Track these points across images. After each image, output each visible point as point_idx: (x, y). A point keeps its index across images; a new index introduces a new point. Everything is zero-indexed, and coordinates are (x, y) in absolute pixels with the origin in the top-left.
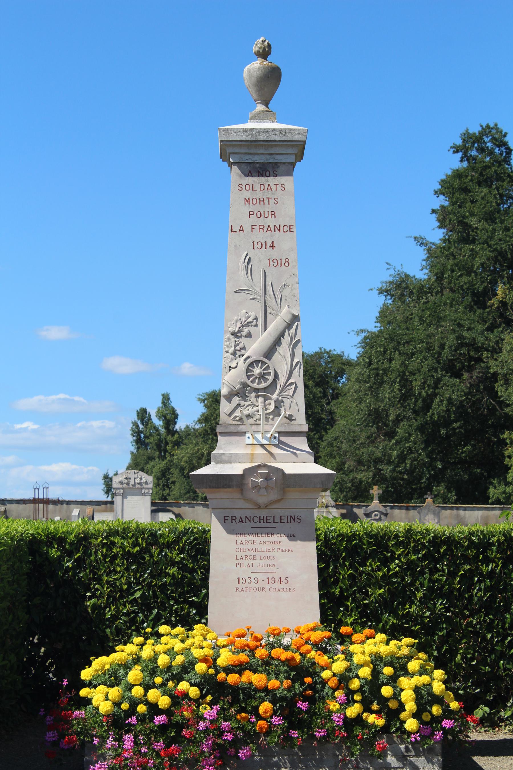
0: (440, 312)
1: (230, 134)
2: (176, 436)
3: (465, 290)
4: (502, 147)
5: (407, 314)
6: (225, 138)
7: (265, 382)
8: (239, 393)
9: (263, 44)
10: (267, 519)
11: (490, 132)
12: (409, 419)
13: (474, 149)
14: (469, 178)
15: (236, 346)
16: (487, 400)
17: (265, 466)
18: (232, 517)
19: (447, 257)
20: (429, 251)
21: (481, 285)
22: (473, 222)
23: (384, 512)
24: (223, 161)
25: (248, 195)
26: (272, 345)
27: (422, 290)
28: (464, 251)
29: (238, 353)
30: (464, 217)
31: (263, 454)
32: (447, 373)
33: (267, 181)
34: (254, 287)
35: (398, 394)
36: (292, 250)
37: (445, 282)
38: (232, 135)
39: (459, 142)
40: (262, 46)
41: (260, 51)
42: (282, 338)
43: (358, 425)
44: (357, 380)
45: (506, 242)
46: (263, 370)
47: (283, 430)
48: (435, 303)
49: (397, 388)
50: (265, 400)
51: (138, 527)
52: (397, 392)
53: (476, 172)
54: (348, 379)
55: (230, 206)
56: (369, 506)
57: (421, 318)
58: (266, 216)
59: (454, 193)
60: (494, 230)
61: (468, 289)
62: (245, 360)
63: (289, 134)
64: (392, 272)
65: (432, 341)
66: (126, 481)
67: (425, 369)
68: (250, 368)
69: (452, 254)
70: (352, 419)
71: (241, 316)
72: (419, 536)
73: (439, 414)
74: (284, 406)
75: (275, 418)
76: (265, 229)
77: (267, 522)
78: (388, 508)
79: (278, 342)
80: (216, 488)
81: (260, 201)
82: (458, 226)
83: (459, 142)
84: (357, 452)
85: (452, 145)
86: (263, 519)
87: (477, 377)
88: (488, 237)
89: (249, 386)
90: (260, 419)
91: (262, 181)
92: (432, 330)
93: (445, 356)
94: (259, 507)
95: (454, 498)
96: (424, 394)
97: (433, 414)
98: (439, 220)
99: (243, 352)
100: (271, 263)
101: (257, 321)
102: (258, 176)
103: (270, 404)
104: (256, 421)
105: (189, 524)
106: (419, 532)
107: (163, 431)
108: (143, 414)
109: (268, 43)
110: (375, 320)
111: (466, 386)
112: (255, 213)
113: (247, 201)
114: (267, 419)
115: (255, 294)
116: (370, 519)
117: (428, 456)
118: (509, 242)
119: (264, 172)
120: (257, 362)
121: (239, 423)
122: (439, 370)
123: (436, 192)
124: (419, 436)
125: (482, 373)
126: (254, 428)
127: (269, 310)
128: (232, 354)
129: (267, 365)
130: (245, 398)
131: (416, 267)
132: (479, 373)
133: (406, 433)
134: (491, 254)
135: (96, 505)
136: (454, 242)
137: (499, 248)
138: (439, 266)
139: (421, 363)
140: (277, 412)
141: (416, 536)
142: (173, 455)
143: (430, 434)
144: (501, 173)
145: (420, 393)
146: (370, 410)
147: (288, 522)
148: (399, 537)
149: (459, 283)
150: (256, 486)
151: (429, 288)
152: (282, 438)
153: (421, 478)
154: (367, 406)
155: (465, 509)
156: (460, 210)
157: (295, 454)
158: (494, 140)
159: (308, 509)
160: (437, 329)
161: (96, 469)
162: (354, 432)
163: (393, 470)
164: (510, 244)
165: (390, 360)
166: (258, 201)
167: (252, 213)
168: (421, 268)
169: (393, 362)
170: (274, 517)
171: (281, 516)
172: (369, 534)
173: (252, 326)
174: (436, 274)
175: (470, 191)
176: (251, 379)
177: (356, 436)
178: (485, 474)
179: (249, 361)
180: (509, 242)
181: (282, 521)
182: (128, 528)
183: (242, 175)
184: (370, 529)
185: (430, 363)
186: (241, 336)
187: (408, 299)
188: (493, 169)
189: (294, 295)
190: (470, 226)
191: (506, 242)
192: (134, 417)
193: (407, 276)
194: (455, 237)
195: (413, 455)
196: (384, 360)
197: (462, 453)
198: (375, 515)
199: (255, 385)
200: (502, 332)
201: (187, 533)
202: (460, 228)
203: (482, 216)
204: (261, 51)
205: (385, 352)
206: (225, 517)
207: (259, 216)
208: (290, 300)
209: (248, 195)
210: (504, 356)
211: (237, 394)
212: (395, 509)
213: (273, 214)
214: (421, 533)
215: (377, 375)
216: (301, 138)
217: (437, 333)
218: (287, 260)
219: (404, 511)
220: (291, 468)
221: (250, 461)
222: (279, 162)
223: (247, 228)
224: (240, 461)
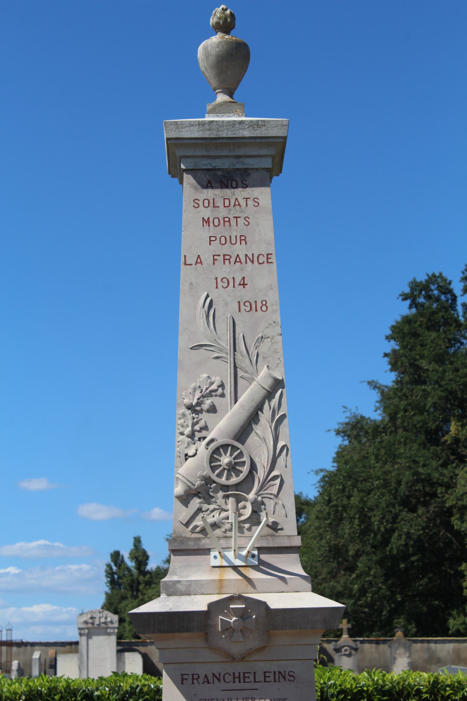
0: (395, 450)
1: (181, 130)
2: (148, 576)
3: (418, 429)
4: (447, 294)
5: (364, 453)
6: (173, 135)
7: (237, 476)
8: (199, 493)
9: (223, 13)
10: (244, 677)
11: (436, 280)
12: (368, 554)
13: (422, 296)
14: (418, 323)
15: (194, 425)
16: (444, 533)
17: (240, 598)
18: (193, 675)
19: (400, 398)
20: (382, 393)
21: (433, 423)
22: (424, 364)
23: (354, 647)
24: (172, 177)
25: (207, 213)
26: (245, 423)
27: (377, 430)
28: (416, 392)
29: (198, 435)
30: (415, 360)
31: (237, 580)
32: (404, 508)
33: (233, 194)
34: (218, 341)
35: (357, 530)
36: (272, 289)
37: (399, 422)
38: (184, 130)
39: (407, 290)
40: (223, 15)
41: (219, 23)
42: (260, 412)
43: (319, 561)
44: (317, 518)
45: (456, 382)
46: (235, 459)
47: (265, 545)
48: (390, 442)
49: (357, 523)
50: (238, 502)
51: (68, 686)
52: (357, 528)
53: (424, 318)
54: (307, 519)
55: (183, 229)
56: (338, 640)
57: (377, 457)
58: (233, 242)
59: (404, 338)
60: (444, 371)
61: (421, 427)
62: (208, 444)
63: (263, 128)
64: (348, 414)
65: (389, 477)
66: (91, 621)
67: (383, 504)
68: (215, 456)
69: (405, 395)
70: (313, 555)
71: (200, 382)
72: (449, 691)
73: (398, 548)
74: (265, 509)
75: (253, 528)
76: (233, 260)
77: (244, 682)
78: (358, 643)
79: (253, 418)
80: (168, 632)
81: (224, 221)
82: (410, 368)
83: (407, 290)
84: (319, 587)
85: (401, 293)
86: (239, 678)
87: (434, 511)
88: (439, 378)
89: (214, 482)
90: (231, 530)
91: (226, 194)
92: (388, 467)
93: (402, 491)
94: (232, 658)
95: (414, 630)
96: (382, 529)
97: (392, 548)
98: (390, 363)
99: (204, 433)
100: (242, 307)
101: (223, 389)
102: (222, 188)
103: (244, 507)
104: (225, 532)
105: (137, 680)
106: (448, 686)
107: (135, 571)
108: (116, 557)
109: (231, 12)
110: (332, 460)
111: (423, 521)
112: (218, 239)
113: (206, 221)
114: (241, 529)
115: (221, 350)
116: (340, 654)
117: (389, 589)
118: (459, 381)
119: (229, 182)
120: (225, 447)
121: (200, 536)
122: (397, 505)
123: (387, 338)
124: (379, 570)
125: (438, 507)
126: (223, 542)
127: (240, 373)
128: (188, 436)
129: (239, 451)
130: (208, 499)
131: (370, 409)
132: (435, 507)
133: (366, 567)
134: (443, 394)
135: (60, 646)
136: (407, 383)
137: (450, 388)
138: (392, 407)
139: (378, 499)
140: (255, 519)
141: (445, 690)
142: (145, 594)
143: (391, 568)
144: (448, 318)
145: (379, 528)
146: (330, 546)
147: (275, 681)
148: (422, 693)
149: (413, 422)
150: (227, 627)
151: (384, 428)
152: (264, 557)
153: (381, 611)
154: (327, 543)
155: (436, 642)
156: (410, 353)
157: (283, 579)
158: (440, 288)
159: (305, 661)
160: (393, 466)
161: (74, 609)
162: (316, 567)
163: (355, 604)
164: (460, 383)
165: (349, 497)
166: (222, 222)
167: (212, 239)
168: (374, 409)
169: (352, 498)
170: (255, 673)
171: (265, 673)
172: (381, 689)
173: (216, 396)
174: (390, 415)
175: (419, 335)
176: (217, 472)
177: (317, 572)
178: (443, 606)
179: (213, 446)
180: (459, 381)
181: (267, 679)
182: (56, 688)
183: (199, 187)
184: (381, 682)
185: (388, 498)
186: (201, 411)
187: (364, 440)
188: (440, 314)
189: (276, 352)
190: (421, 368)
191: (456, 382)
192: (108, 560)
193: (362, 417)
194: (407, 378)
195: (374, 589)
196: (343, 497)
197: (419, 585)
198: (346, 650)
199: (223, 481)
200: (456, 468)
201: (134, 693)
202: (411, 370)
203: (432, 358)
204: (221, 22)
205: (344, 490)
206: (182, 675)
207: (223, 242)
208: (270, 359)
209: (207, 213)
210: (459, 490)
211: (197, 494)
212: (365, 643)
213: (243, 239)
214: (451, 686)
215: (337, 512)
216: (281, 133)
217: (394, 470)
218: (264, 303)
219: (374, 645)
220: (277, 601)
221: (218, 592)
222: (250, 167)
223: (207, 259)
224: (203, 591)
